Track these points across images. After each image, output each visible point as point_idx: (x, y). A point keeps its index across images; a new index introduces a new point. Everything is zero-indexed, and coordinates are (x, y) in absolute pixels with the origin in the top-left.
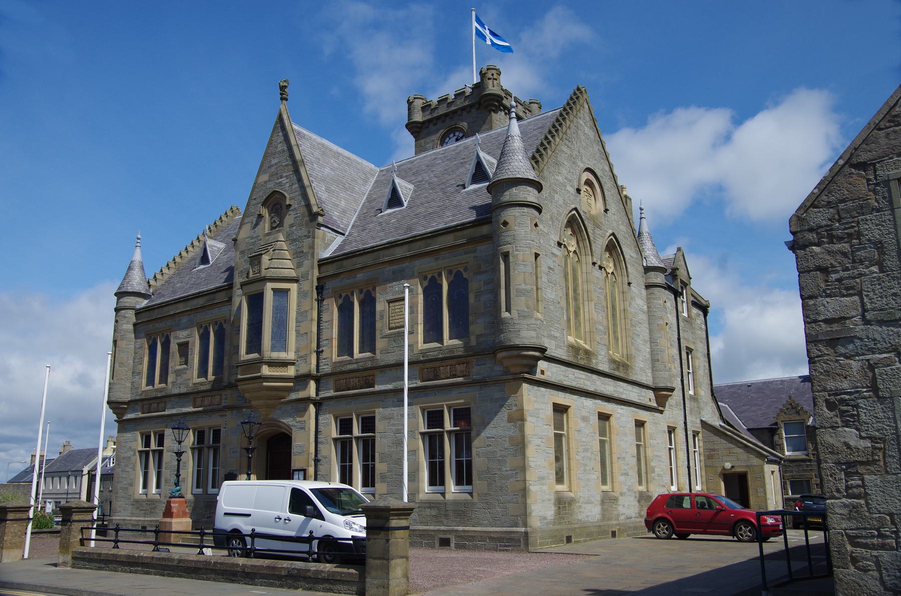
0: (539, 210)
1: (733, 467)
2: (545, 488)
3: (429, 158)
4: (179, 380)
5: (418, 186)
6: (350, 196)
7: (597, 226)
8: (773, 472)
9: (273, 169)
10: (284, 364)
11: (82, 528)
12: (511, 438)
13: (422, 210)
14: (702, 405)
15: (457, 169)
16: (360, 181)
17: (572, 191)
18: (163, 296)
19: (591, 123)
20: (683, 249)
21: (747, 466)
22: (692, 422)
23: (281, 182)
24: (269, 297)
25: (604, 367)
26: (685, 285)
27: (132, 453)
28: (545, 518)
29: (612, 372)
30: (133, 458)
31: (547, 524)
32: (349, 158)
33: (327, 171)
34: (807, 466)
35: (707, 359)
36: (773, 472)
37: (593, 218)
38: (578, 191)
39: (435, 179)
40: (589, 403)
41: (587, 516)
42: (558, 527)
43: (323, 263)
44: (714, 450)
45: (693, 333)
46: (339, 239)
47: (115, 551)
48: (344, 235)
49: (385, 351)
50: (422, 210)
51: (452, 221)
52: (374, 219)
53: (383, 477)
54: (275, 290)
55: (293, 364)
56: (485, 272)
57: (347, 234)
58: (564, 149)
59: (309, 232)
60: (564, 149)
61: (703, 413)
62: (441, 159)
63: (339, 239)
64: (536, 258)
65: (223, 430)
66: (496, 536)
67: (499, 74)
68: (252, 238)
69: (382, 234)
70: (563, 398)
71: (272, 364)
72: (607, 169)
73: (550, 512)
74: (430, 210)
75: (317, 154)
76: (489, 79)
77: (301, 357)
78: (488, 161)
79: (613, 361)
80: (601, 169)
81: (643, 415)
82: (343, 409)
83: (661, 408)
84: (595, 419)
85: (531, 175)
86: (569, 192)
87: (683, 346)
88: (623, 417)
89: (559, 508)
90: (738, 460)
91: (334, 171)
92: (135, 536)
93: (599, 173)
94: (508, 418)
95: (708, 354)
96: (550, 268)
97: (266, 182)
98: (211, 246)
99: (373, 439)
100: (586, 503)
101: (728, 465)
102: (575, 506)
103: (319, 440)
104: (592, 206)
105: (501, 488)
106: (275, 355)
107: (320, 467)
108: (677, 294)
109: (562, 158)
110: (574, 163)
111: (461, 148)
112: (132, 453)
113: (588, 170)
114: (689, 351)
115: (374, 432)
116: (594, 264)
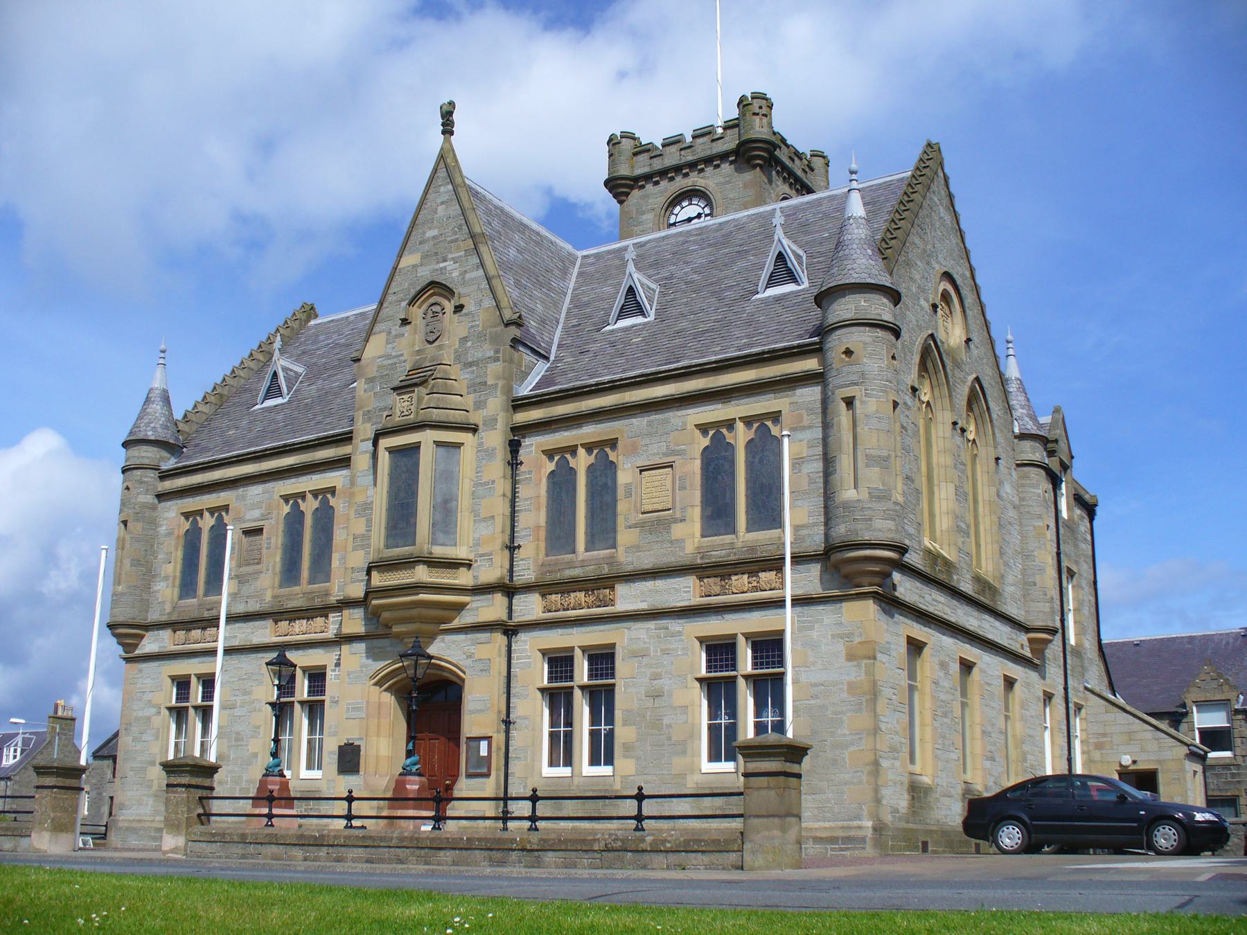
0: (897, 333)
1: (1134, 762)
2: (897, 764)
3: (673, 241)
4: (246, 590)
5: (666, 283)
6: (547, 295)
7: (958, 365)
8: (1195, 772)
9: (426, 247)
10: (453, 564)
11: (201, 798)
12: (851, 687)
13: (684, 324)
14: (1086, 663)
15: (733, 262)
16: (557, 272)
17: (927, 306)
18: (208, 450)
19: (946, 201)
20: (1063, 409)
21: (1159, 762)
22: (1074, 689)
23: (445, 268)
24: (427, 456)
25: (967, 587)
26: (1065, 467)
27: (154, 710)
28: (897, 811)
29: (976, 596)
30: (157, 721)
31: (900, 818)
32: (538, 234)
33: (513, 252)
34: (1233, 775)
35: (1092, 591)
36: (1195, 772)
37: (951, 352)
38: (935, 307)
39: (696, 277)
40: (948, 641)
41: (946, 816)
42: (911, 826)
43: (519, 404)
44: (1104, 735)
45: (1076, 546)
46: (541, 368)
47: (270, 830)
48: (547, 358)
49: (630, 549)
50: (684, 324)
51: (750, 346)
52: (597, 335)
53: (627, 747)
54: (392, 451)
55: (469, 566)
56: (810, 427)
57: (552, 358)
58: (917, 241)
59: (497, 351)
60: (917, 241)
61: (1087, 676)
62: (695, 242)
63: (541, 368)
64: (895, 408)
65: (330, 675)
66: (824, 835)
67: (771, 107)
68: (388, 357)
69: (621, 361)
70: (920, 631)
71: (434, 563)
72: (968, 274)
73: (903, 803)
74: (702, 327)
75: (495, 223)
76: (754, 114)
77: (482, 555)
78: (793, 252)
79: (978, 579)
80: (960, 273)
81: (1015, 671)
82: (557, 639)
83: (1036, 661)
84: (955, 667)
85: (886, 280)
86: (922, 308)
87: (1065, 564)
88: (990, 666)
89: (913, 798)
90: (1143, 750)
91: (521, 253)
92: (499, 749)
93: (959, 281)
94: (847, 655)
95: (1095, 583)
96: (903, 427)
97: (414, 266)
98: (285, 369)
99: (610, 690)
100: (945, 796)
101: (1126, 760)
102: (931, 798)
103: (513, 691)
104: (953, 333)
105: (834, 762)
106: (439, 551)
107: (513, 733)
108: (1055, 481)
109: (913, 254)
110: (928, 264)
111: (730, 228)
112: (154, 710)
113: (947, 276)
114: (1071, 574)
115: (613, 676)
116: (955, 424)
